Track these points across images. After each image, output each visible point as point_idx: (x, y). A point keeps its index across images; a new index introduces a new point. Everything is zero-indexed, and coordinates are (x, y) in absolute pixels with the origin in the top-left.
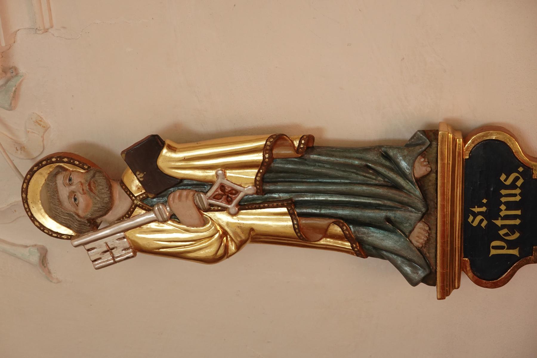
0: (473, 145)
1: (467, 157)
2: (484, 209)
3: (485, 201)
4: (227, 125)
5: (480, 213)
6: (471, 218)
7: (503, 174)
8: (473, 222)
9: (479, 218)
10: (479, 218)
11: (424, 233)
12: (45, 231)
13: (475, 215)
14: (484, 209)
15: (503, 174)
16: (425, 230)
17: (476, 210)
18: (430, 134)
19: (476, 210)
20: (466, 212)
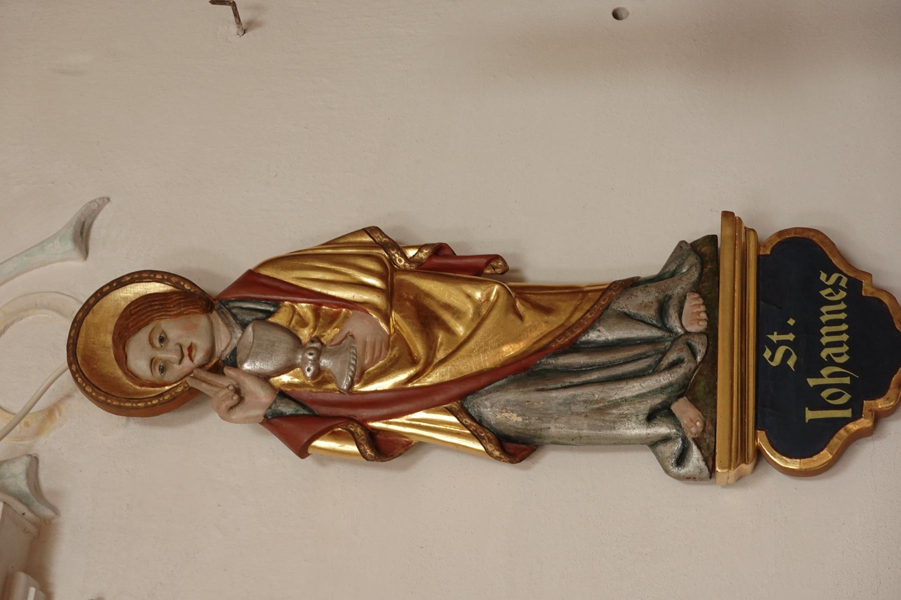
0: (779, 240)
1: (768, 253)
2: (791, 337)
3: (791, 322)
4: (38, 394)
5: (781, 343)
6: (767, 354)
7: (850, 410)
8: (772, 358)
9: (781, 351)
10: (781, 351)
11: (697, 302)
12: (108, 288)
13: (774, 347)
14: (791, 337)
15: (850, 410)
16: (696, 299)
17: (775, 337)
18: (703, 254)
19: (775, 337)
20: (762, 343)
